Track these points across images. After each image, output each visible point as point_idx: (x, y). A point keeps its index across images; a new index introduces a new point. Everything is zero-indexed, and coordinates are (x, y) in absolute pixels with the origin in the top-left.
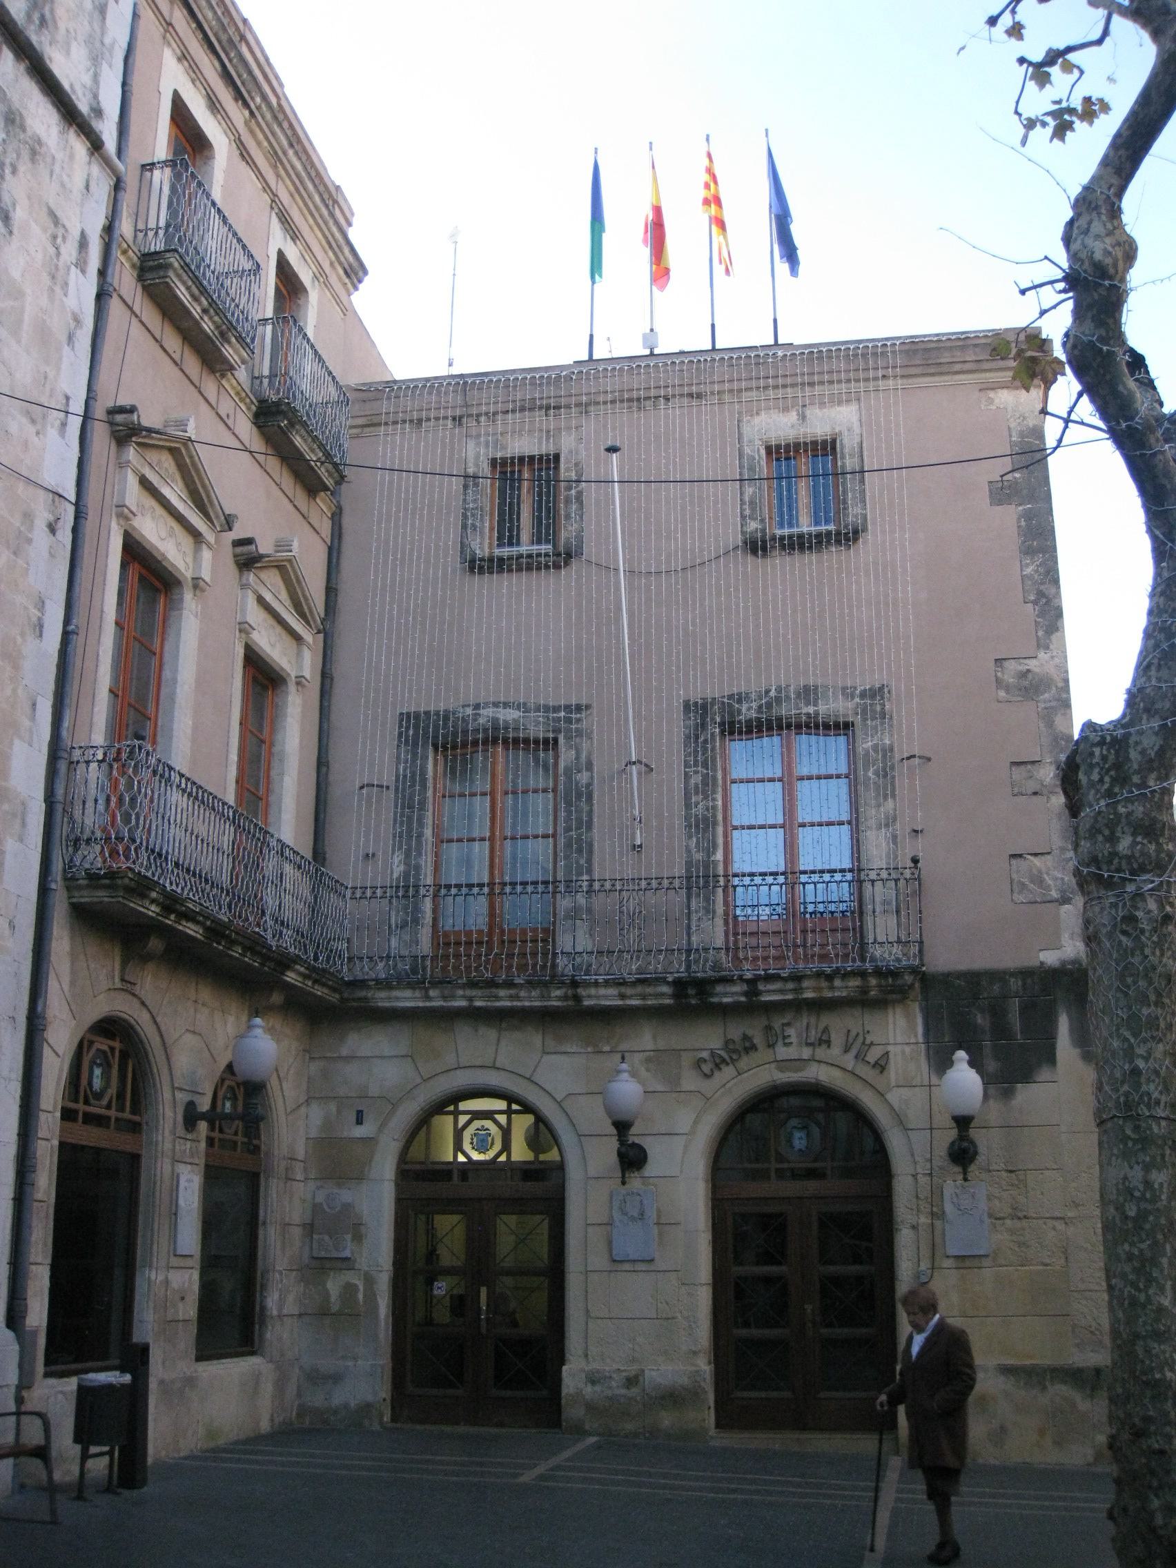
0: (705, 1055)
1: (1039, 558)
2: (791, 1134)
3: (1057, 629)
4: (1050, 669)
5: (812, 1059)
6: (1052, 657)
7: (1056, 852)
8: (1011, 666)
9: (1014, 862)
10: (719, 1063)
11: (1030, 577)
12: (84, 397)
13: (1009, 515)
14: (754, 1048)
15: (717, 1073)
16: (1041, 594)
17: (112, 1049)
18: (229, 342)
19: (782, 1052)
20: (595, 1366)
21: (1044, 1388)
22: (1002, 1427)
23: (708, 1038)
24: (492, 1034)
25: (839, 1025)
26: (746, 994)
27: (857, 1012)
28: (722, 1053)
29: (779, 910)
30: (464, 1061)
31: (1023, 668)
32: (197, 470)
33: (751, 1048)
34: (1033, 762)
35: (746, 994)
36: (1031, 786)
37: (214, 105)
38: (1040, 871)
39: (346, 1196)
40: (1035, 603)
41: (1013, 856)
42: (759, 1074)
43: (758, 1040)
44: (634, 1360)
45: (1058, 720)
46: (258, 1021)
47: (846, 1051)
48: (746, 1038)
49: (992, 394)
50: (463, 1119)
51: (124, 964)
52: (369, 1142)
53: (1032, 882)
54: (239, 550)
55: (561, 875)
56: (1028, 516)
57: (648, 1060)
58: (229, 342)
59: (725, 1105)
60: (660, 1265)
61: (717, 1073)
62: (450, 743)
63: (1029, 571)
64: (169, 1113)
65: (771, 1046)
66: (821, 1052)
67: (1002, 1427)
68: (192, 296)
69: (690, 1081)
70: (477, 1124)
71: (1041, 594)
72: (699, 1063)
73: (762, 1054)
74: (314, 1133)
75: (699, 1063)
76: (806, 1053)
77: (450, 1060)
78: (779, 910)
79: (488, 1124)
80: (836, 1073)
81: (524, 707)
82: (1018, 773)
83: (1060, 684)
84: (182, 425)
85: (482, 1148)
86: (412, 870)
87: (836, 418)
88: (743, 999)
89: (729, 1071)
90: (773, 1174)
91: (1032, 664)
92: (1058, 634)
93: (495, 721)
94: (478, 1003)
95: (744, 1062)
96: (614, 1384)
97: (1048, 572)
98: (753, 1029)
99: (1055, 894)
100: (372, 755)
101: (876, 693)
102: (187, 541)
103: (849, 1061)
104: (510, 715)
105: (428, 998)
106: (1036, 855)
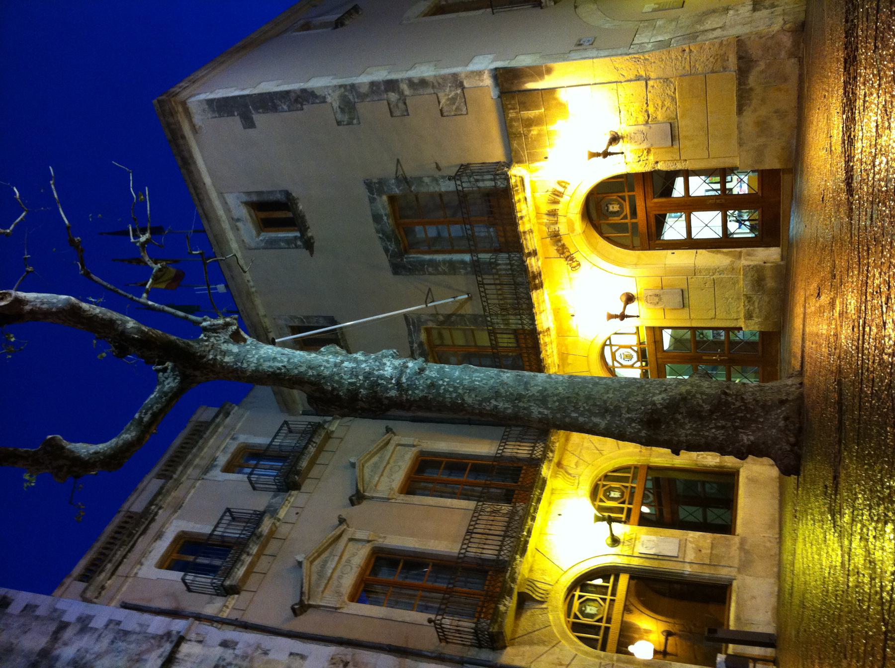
1: (278, 102)
3: (313, 92)
7: (436, 91)
8: (340, 116)
9: (445, 114)
11: (289, 107)
13: (259, 118)
16: (296, 101)
17: (580, 597)
20: (742, 315)
21: (751, 89)
22: (775, 112)
29: (509, 106)
31: (339, 110)
34: (389, 104)
36: (401, 105)
37: (159, 536)
38: (448, 99)
40: (302, 105)
41: (442, 115)
44: (739, 299)
49: (197, 127)
50: (616, 364)
53: (454, 104)
55: (438, 606)
56: (256, 109)
60: (685, 287)
63: (285, 107)
67: (775, 112)
70: (618, 358)
71: (296, 101)
78: (509, 106)
79: (617, 354)
82: (397, 113)
83: (342, 90)
85: (631, 357)
90: (634, 221)
91: (336, 105)
96: (752, 308)
97: (284, 97)
99: (459, 91)
101: (369, 185)
106: (439, 102)
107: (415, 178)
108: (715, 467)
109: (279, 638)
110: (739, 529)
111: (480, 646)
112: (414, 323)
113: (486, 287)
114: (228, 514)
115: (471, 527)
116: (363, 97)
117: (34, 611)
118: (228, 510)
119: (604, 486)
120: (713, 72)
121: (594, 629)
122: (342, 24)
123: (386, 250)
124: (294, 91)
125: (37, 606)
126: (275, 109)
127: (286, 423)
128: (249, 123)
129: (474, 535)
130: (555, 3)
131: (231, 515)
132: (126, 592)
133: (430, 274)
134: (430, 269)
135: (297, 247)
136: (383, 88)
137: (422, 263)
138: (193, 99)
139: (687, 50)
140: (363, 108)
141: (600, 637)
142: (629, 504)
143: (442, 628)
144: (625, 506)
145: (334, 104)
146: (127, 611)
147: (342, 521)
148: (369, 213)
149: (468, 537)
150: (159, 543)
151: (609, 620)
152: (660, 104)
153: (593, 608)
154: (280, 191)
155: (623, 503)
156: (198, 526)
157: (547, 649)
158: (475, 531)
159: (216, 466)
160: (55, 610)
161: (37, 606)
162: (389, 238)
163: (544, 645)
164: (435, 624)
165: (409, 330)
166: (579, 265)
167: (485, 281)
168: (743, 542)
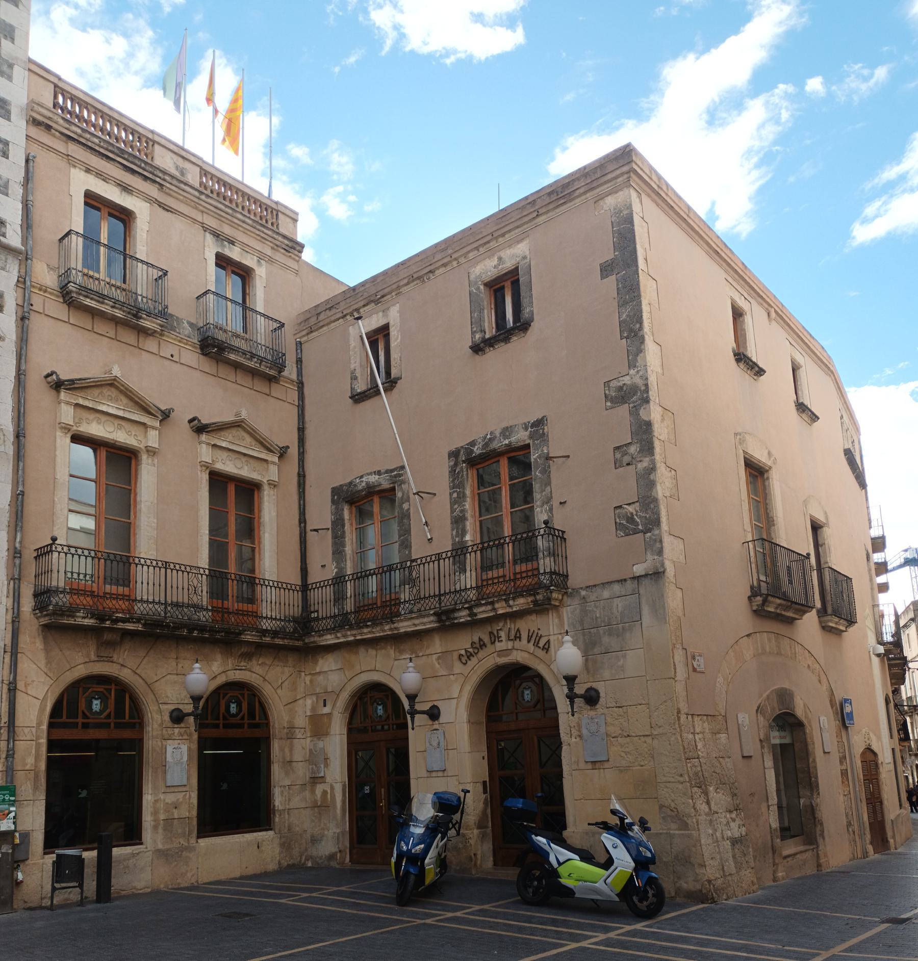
0: (463, 652)
2: (523, 692)
4: (638, 381)
5: (513, 648)
6: (638, 372)
10: (470, 656)
12: (13, 374)
14: (485, 645)
15: (469, 662)
18: (141, 318)
19: (499, 646)
23: (463, 642)
24: (372, 652)
25: (526, 625)
26: (469, 615)
27: (533, 617)
28: (471, 650)
30: (363, 669)
31: (621, 384)
32: (130, 392)
33: (483, 645)
35: (469, 615)
36: (627, 459)
37: (126, 189)
38: (632, 514)
39: (321, 744)
40: (627, 338)
42: (488, 660)
43: (486, 639)
45: (642, 413)
46: (197, 665)
47: (529, 642)
48: (480, 640)
51: (98, 648)
52: (329, 715)
54: (192, 424)
57: (439, 658)
58: (141, 318)
59: (475, 679)
61: (469, 662)
62: (358, 500)
64: (157, 717)
65: (493, 643)
66: (517, 644)
68: (98, 302)
69: (458, 668)
71: (631, 330)
72: (460, 656)
73: (490, 649)
74: (308, 713)
75: (460, 656)
76: (510, 645)
77: (358, 669)
80: (526, 655)
81: (379, 473)
83: (643, 388)
84: (110, 372)
86: (341, 569)
87: (513, 254)
88: (469, 619)
89: (474, 660)
91: (627, 380)
92: (641, 355)
93: (367, 483)
94: (359, 637)
95: (481, 654)
98: (481, 634)
100: (321, 513)
102: (135, 430)
103: (531, 648)
104: (373, 479)
105: (338, 638)
106: (629, 504)
107: (549, 476)
108: (274, 806)
109: (15, 362)
110: (204, 842)
111: (36, 595)
112: (400, 475)
113: (436, 563)
114: (160, 273)
115: (172, 566)
116: (634, 412)
117: (6, 37)
118: (166, 273)
119: (243, 695)
120: (661, 807)
121: (73, 713)
122: (738, 360)
123: (473, 443)
124: (641, 328)
125: (13, 40)
126: (622, 304)
127: (283, 325)
128: (606, 270)
129: (163, 570)
130: (755, 611)
131: (160, 277)
132: (45, 162)
133: (451, 494)
134: (455, 495)
135: (473, 333)
136: (645, 437)
137: (461, 485)
138: (634, 194)
139: (681, 779)
140: (624, 410)
141: (64, 719)
142: (224, 725)
143: (48, 552)
144: (221, 722)
145: (628, 378)
146: (23, 164)
147: (166, 415)
148: (511, 423)
149: (160, 564)
150: (117, 190)
151: (85, 726)
152: (627, 750)
153: (98, 707)
154: (532, 312)
155: (225, 718)
156: (145, 235)
157: (43, 667)
158: (169, 571)
159: (223, 246)
160: (11, 66)
161: (13, 40)
162: (486, 445)
163: (47, 664)
164: (51, 545)
165: (392, 471)
166: (465, 664)
167: (442, 561)
168: (190, 849)
